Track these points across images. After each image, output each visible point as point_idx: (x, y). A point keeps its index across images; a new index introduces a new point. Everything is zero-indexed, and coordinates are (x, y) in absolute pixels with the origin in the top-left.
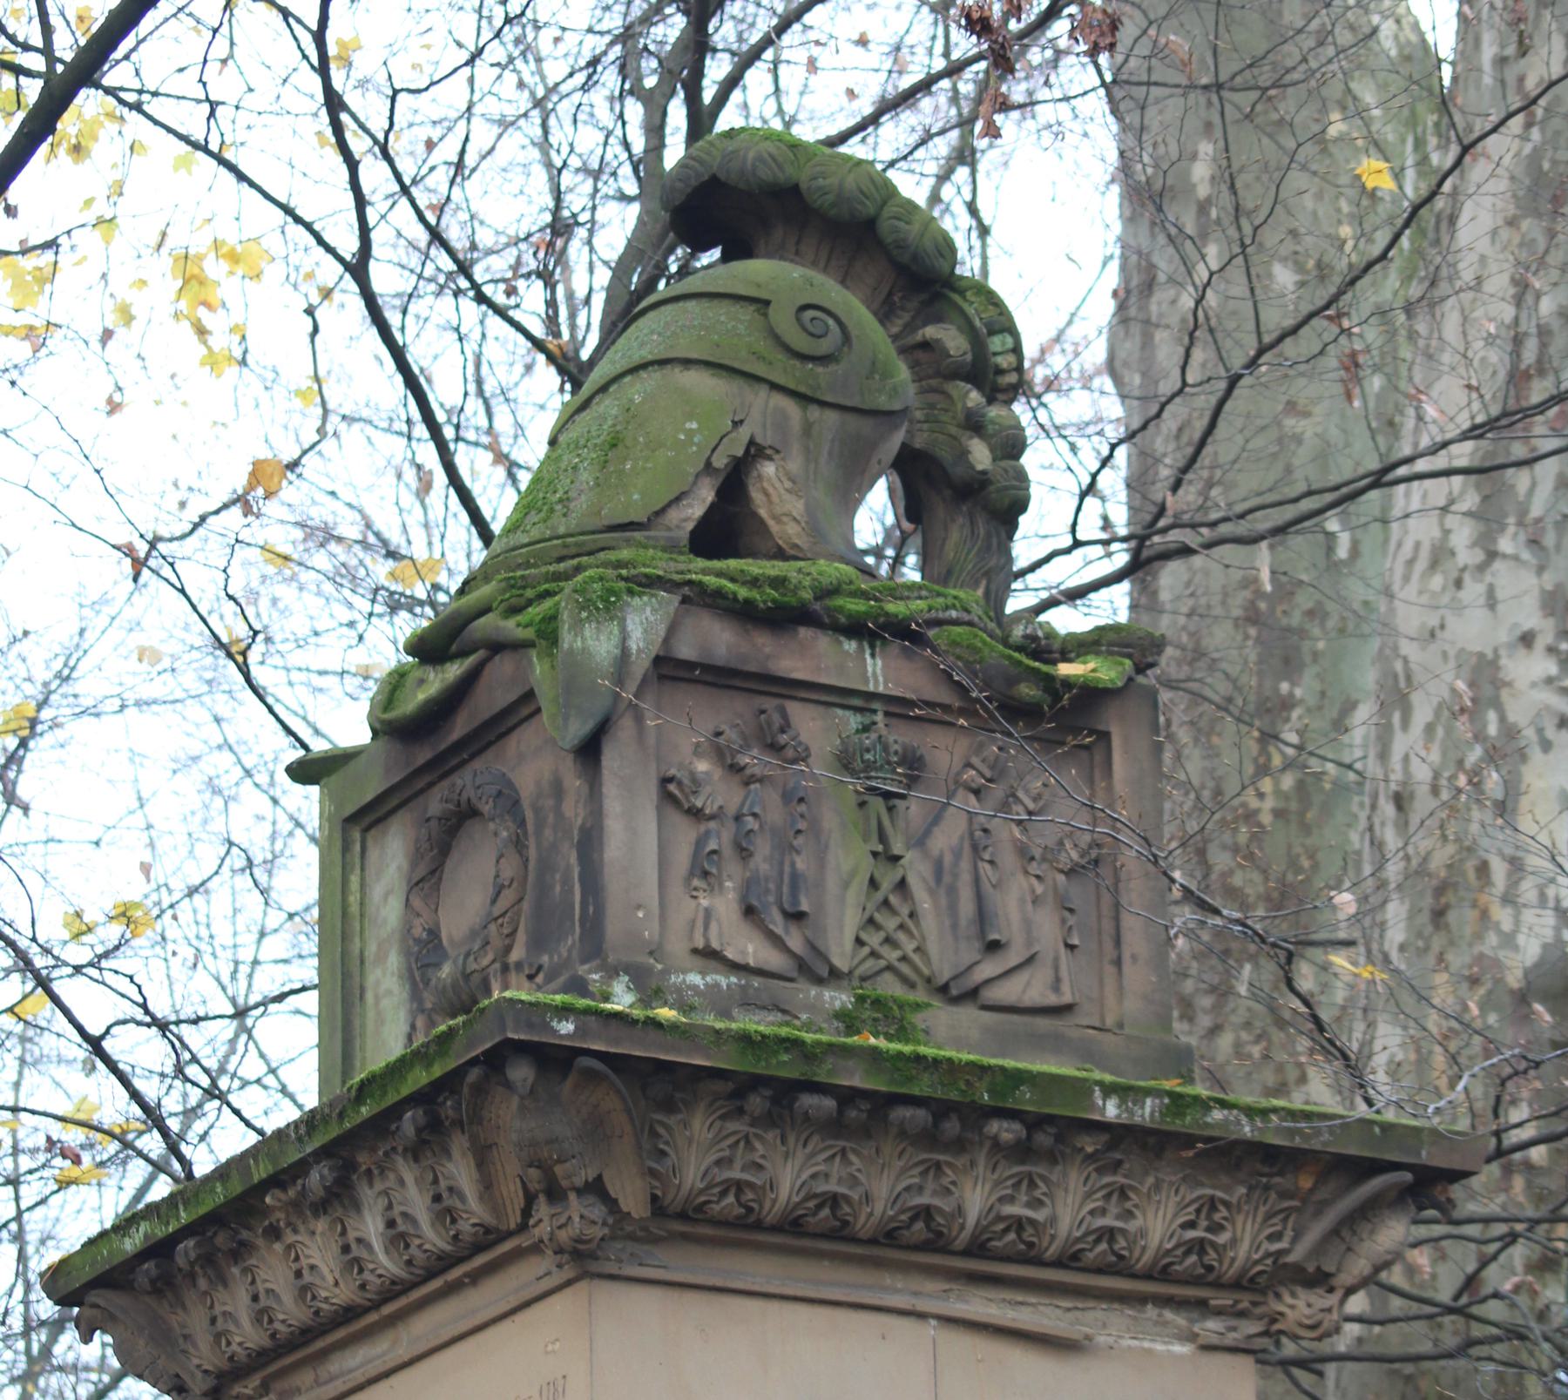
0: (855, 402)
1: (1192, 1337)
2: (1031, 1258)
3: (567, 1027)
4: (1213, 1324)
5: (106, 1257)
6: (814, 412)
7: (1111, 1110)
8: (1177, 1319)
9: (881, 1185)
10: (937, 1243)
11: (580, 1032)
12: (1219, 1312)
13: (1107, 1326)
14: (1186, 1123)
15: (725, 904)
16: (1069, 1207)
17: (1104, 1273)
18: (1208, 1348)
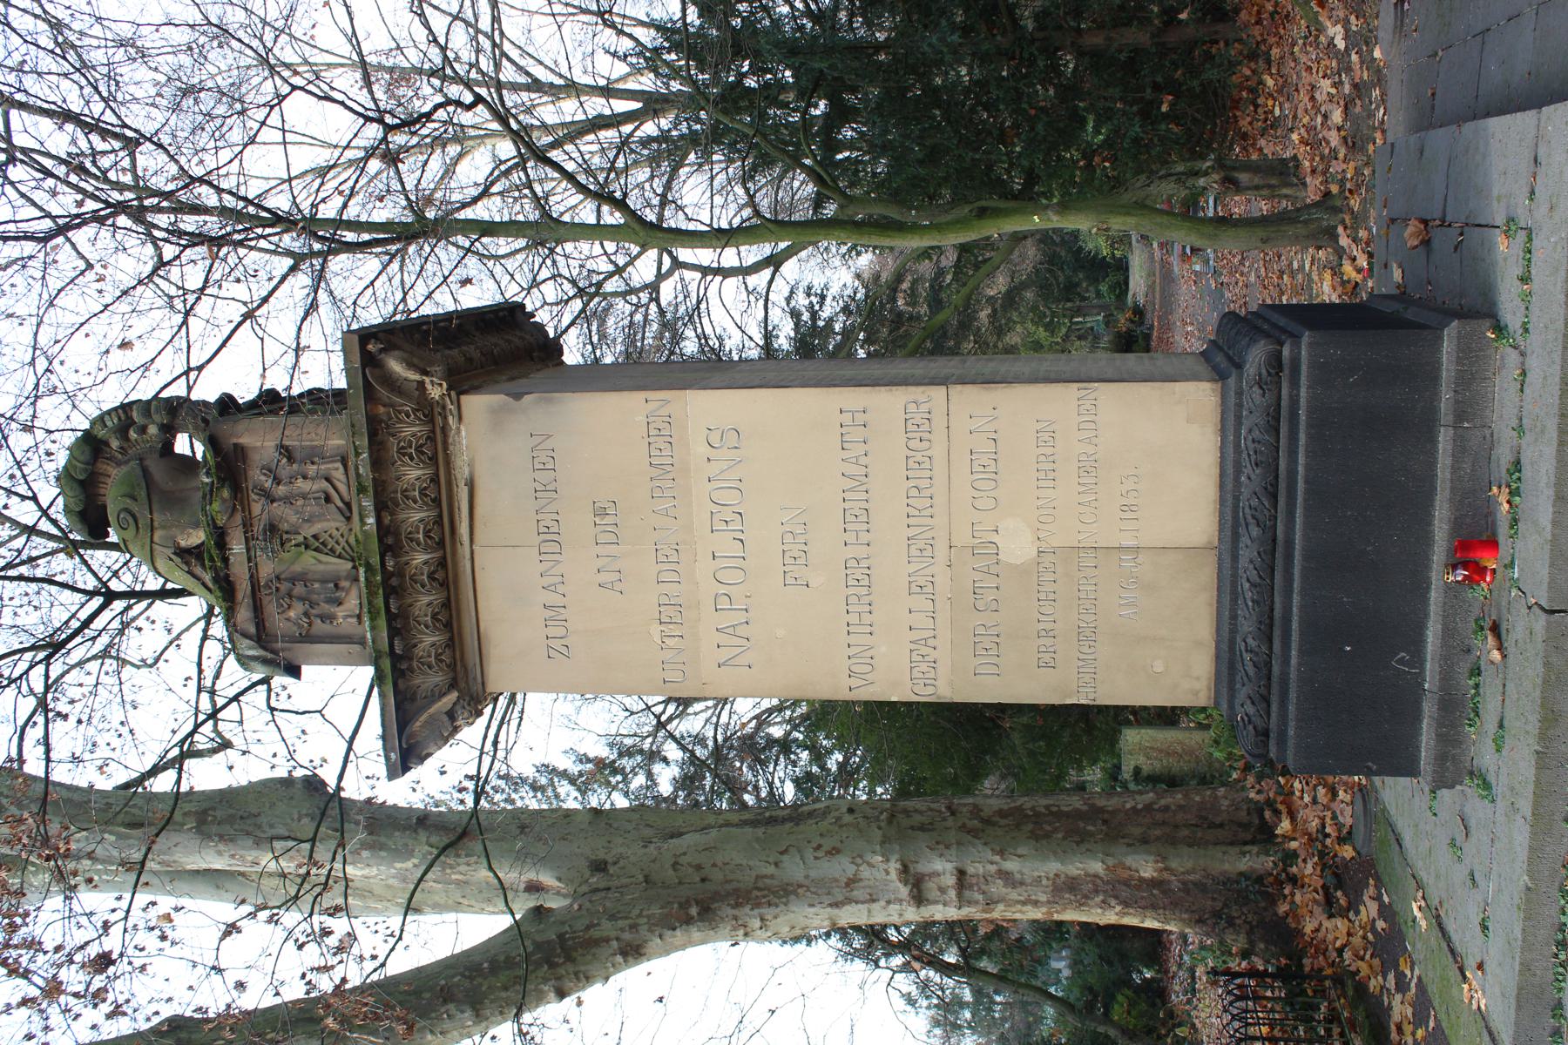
2: (439, 521)
5: (1253, 419)
7: (371, 520)
9: (424, 602)
10: (442, 563)
12: (445, 418)
13: (461, 471)
14: (369, 483)
15: (340, 612)
16: (415, 516)
18: (460, 418)
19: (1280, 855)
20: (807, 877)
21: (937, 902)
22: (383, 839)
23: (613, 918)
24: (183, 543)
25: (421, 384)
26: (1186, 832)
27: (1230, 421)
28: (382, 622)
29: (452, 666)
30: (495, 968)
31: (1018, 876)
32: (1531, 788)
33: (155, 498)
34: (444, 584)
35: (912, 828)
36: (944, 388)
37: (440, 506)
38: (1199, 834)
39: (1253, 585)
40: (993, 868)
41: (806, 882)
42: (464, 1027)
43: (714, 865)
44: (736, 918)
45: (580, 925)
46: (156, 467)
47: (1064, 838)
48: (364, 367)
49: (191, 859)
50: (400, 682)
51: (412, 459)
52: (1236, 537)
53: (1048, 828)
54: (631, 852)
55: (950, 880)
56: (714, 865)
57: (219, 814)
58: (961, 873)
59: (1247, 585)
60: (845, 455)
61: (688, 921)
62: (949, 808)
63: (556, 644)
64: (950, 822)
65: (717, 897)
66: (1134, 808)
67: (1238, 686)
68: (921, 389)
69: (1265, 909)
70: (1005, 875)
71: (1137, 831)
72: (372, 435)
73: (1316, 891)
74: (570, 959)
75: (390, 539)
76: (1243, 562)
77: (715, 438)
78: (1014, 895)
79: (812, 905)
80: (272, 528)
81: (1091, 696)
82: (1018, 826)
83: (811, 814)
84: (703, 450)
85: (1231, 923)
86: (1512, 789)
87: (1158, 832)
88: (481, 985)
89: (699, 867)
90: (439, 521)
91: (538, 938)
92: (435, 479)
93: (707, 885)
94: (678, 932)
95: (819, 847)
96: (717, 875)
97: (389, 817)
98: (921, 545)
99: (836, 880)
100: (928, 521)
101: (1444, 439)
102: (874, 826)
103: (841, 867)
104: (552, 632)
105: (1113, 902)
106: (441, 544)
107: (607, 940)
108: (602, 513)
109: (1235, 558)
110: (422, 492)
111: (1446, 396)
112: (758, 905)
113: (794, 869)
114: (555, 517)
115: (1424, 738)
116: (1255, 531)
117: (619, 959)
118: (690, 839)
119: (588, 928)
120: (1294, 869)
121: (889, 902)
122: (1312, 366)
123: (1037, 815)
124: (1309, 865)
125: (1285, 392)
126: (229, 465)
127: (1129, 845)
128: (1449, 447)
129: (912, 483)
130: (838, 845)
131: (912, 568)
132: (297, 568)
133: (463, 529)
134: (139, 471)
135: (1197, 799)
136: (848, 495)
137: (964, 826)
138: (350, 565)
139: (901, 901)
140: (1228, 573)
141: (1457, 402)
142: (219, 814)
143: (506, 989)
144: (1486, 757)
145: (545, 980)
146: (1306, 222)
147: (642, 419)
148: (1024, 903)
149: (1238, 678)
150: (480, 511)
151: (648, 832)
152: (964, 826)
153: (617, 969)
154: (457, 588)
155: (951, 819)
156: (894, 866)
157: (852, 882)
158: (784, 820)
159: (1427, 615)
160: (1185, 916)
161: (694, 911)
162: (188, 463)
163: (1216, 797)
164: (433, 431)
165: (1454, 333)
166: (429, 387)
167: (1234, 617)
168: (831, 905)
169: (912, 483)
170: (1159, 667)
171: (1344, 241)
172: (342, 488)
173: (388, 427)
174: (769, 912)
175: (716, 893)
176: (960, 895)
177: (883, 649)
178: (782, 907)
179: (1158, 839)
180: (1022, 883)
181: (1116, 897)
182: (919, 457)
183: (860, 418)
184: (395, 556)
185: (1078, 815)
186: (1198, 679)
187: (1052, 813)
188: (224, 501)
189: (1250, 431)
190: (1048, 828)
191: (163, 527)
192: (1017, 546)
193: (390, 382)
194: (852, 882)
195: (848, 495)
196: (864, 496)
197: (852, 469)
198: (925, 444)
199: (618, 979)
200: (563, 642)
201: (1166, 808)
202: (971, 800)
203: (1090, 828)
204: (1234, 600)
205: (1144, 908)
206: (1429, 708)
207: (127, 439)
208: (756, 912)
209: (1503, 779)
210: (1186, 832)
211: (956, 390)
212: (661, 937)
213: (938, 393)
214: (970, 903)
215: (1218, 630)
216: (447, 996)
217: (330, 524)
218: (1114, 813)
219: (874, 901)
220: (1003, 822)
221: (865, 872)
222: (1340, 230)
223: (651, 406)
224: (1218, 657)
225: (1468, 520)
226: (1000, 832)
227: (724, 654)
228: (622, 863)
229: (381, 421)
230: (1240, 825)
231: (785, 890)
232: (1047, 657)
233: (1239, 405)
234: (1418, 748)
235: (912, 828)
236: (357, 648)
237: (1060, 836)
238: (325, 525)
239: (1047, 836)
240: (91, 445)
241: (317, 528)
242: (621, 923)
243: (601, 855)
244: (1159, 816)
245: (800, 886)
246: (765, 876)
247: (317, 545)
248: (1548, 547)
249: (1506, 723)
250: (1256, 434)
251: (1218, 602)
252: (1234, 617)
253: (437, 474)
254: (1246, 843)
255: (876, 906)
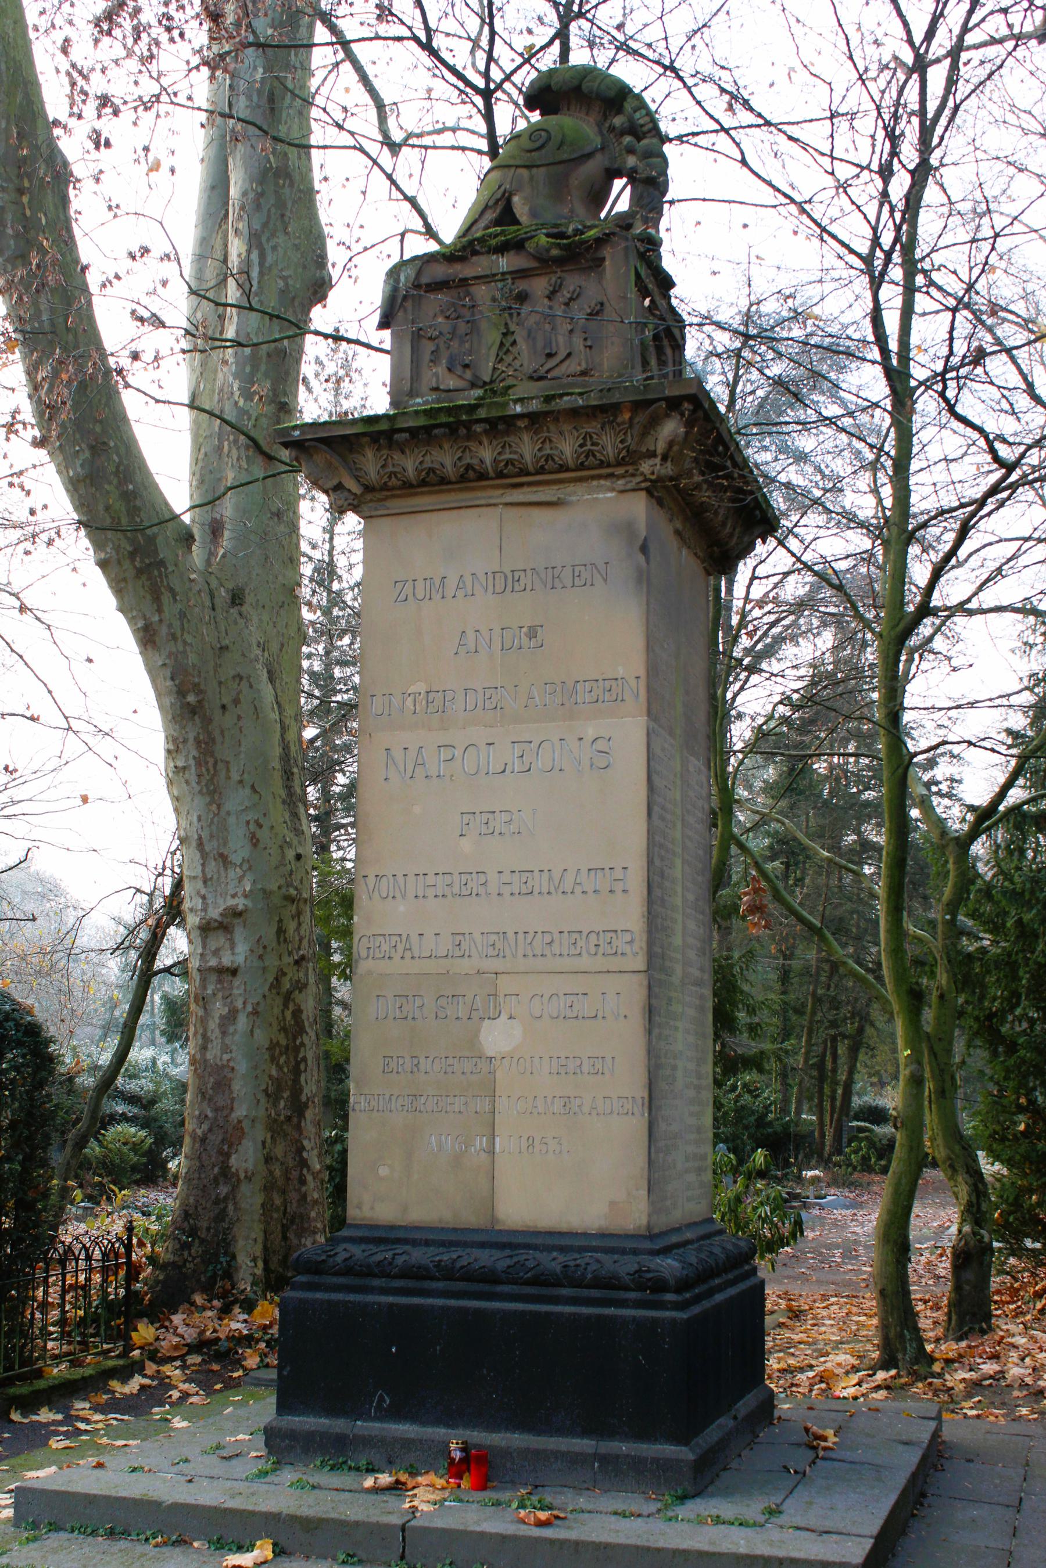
0: (551, 160)
1: (613, 490)
2: (524, 472)
3: (297, 433)
4: (620, 482)
6: (534, 170)
7: (518, 409)
8: (606, 483)
9: (445, 459)
10: (482, 476)
11: (302, 433)
12: (623, 476)
14: (554, 405)
15: (441, 369)
16: (526, 448)
17: (549, 470)
18: (622, 492)
19: (252, 1296)
20: (228, 813)
21: (204, 946)
22: (263, 367)
23: (182, 615)
24: (516, 199)
25: (652, 454)
26: (278, 1201)
27: (609, 1243)
28: (422, 421)
29: (385, 487)
30: (129, 497)
31: (231, 1029)
32: (250, 1508)
33: (560, 168)
34: (463, 479)
35: (280, 921)
36: (643, 968)
37: (537, 473)
38: (275, 1215)
39: (454, 1261)
40: (239, 1004)
41: (223, 813)
42: (66, 468)
43: (239, 718)
44: (185, 741)
45: (176, 583)
46: (593, 167)
47: (270, 1077)
48: (667, 399)
49: (239, 163)
50: (367, 439)
51: (581, 446)
52: (502, 1246)
53: (282, 1060)
54: (255, 628)
55: (227, 961)
56: (239, 718)
57: (287, 191)
58: (234, 972)
59: (455, 1256)
60: (584, 871)
61: (181, 693)
62: (303, 958)
63: (408, 589)
64: (288, 960)
65: (207, 721)
66: (303, 1148)
67: (363, 1246)
68: (644, 945)
69: (198, 1281)
70: (232, 1015)
71: (279, 1151)
72: (602, 409)
73: (215, 1331)
74: (140, 572)
75: (502, 426)
76: (477, 1253)
77: (600, 745)
78: (213, 1025)
79: (199, 819)
80: (522, 297)
81: (357, 1107)
82: (283, 1029)
83: (295, 815)
84: (591, 733)
85: (185, 1246)
86: (253, 1494)
87: (277, 1173)
88: (110, 483)
89: (236, 702)
90: (524, 472)
91: (160, 540)
92: (563, 468)
93: (218, 712)
94: (169, 683)
95: (260, 826)
96: (229, 720)
97: (287, 373)
98: (498, 946)
99: (225, 844)
100: (520, 953)
101: (584, 1445)
102: (282, 881)
103: (239, 849)
104: (420, 584)
105: (205, 1127)
106: (500, 475)
107: (160, 610)
108: (532, 633)
109: (483, 1245)
110: (549, 457)
111: (623, 1447)
112: (198, 764)
113: (236, 800)
114: (529, 588)
115: (312, 1420)
116: (502, 1265)
117: (140, 624)
118: (267, 692)
119: (172, 590)
120: (237, 1310)
121: (204, 898)
122: (655, 1321)
123: (297, 1049)
124: (239, 1326)
125: (633, 1295)
126: (578, 254)
127: (264, 1143)
128: (577, 1449)
129: (556, 936)
130: (261, 845)
131: (477, 936)
132: (484, 325)
133: (517, 495)
134: (588, 150)
135: (313, 1214)
136: (546, 875)
137: (284, 974)
138: (487, 379)
139: (205, 910)
140: (469, 1238)
141: (618, 1456)
142: (287, 191)
143: (107, 508)
144: (288, 1475)
145: (117, 549)
146: (901, 1336)
147: (621, 672)
148: (204, 1036)
149: (371, 1246)
150: (535, 512)
151: (274, 647)
152: (284, 974)
153: (131, 621)
154: (461, 490)
155: (291, 960)
156: (240, 903)
157: (224, 859)
158: (289, 788)
159: (424, 1424)
160: (192, 1200)
161: (191, 698)
162: (599, 195)
163: (315, 1233)
164: (609, 465)
165: (681, 1456)
166: (651, 462)
167: (427, 1243)
168: (200, 838)
169: (556, 936)
170: (383, 1171)
171: (881, 1375)
172: (563, 369)
173: (611, 423)
174: (192, 775)
175: (210, 720)
176: (211, 969)
177: (402, 908)
178: (197, 788)
179: (271, 1173)
180: (224, 1033)
181: (210, 1130)
182: (580, 943)
183: (619, 887)
184: (485, 431)
185: (296, 1090)
186: (372, 1208)
187: (298, 1064)
188: (548, 250)
189: (598, 1261)
190: (282, 1060)
191: (531, 178)
192: (498, 1037)
193: (654, 422)
194: (224, 859)
195: (546, 875)
196: (545, 890)
197: (570, 878)
198: (593, 950)
199: (121, 620)
200: (410, 597)
201: (303, 1182)
202: (312, 980)
203: (282, 1104)
204: (443, 1244)
205: (199, 1158)
206: (339, 1425)
207: (622, 134)
208: (192, 762)
209: (266, 1487)
210: (278, 1201)
211: (643, 979)
212: (164, 665)
213: (639, 963)
214: (204, 981)
215: (417, 1228)
216: (98, 448)
217: (526, 358)
218: (298, 1128)
219: (205, 882)
220: (288, 1014)
221: (233, 874)
222: (893, 1372)
223: (633, 683)
224: (392, 1228)
225: (509, 1464)
226: (277, 1011)
227: (398, 754)
228: (242, 621)
229: (616, 417)
230: (286, 1257)
231: (215, 791)
232: (393, 1065)
233: (623, 1252)
234: (303, 1414)
235: (280, 921)
236: (407, 387)
237: (274, 1073)
238: (525, 354)
239: (273, 1059)
240: (617, 99)
241: (522, 345)
242: (177, 623)
243: (250, 599)
244: (295, 1174)
245: (219, 807)
246: (228, 770)
247: (506, 345)
248: (462, 1527)
249: (317, 1491)
250: (594, 1266)
251: (443, 1229)
252: (427, 1243)
253: (568, 470)
254: (266, 1262)
255: (200, 884)
